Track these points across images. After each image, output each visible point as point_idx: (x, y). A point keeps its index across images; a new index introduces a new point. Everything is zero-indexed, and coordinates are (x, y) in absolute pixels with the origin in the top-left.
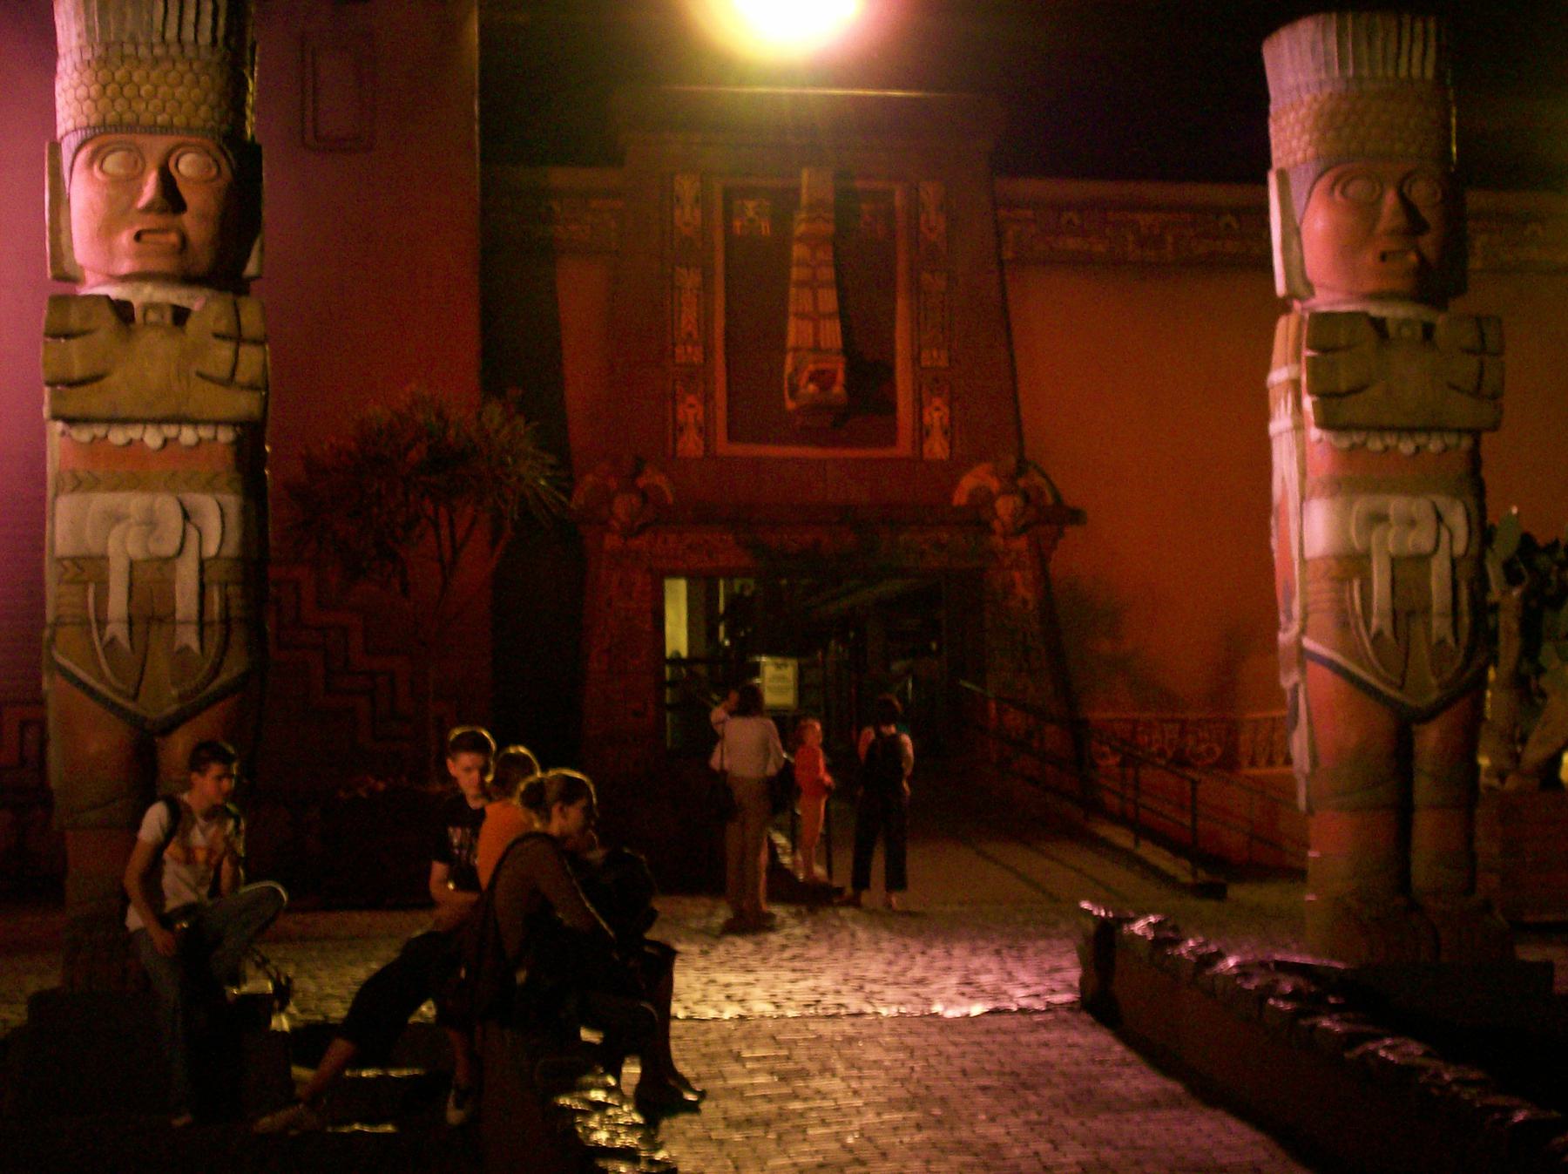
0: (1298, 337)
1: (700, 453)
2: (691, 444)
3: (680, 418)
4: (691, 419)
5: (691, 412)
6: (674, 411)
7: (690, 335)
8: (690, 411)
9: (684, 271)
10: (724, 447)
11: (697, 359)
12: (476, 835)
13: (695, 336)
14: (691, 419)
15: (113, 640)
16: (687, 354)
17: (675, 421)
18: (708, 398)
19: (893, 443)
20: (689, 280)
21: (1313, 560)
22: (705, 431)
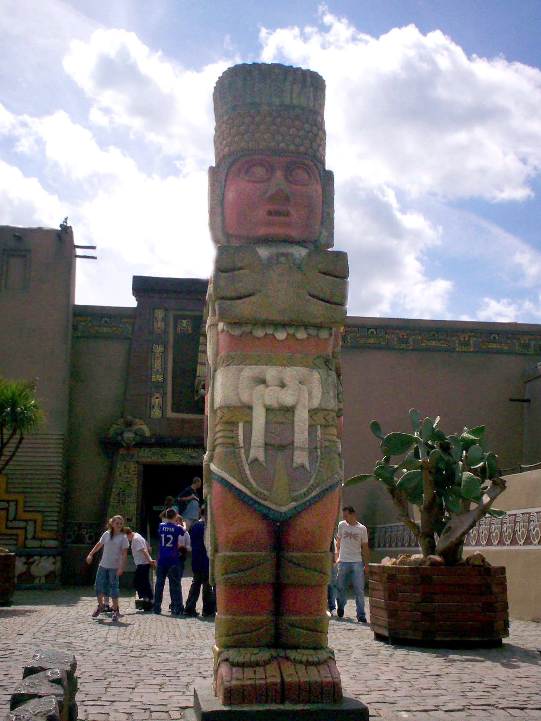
0: (28, 589)
1: (160, 416)
2: (156, 413)
3: (153, 402)
4: (157, 403)
5: (157, 400)
6: (151, 400)
7: (158, 371)
8: (156, 401)
9: (157, 346)
10: (170, 414)
11: (161, 380)
12: (354, 563)
13: (160, 371)
14: (157, 403)
15: (256, 460)
16: (157, 378)
17: (151, 404)
18: (165, 394)
19: (173, 410)
20: (159, 349)
21: (75, 249)
22: (162, 408)
